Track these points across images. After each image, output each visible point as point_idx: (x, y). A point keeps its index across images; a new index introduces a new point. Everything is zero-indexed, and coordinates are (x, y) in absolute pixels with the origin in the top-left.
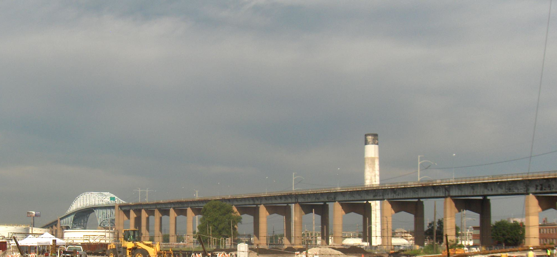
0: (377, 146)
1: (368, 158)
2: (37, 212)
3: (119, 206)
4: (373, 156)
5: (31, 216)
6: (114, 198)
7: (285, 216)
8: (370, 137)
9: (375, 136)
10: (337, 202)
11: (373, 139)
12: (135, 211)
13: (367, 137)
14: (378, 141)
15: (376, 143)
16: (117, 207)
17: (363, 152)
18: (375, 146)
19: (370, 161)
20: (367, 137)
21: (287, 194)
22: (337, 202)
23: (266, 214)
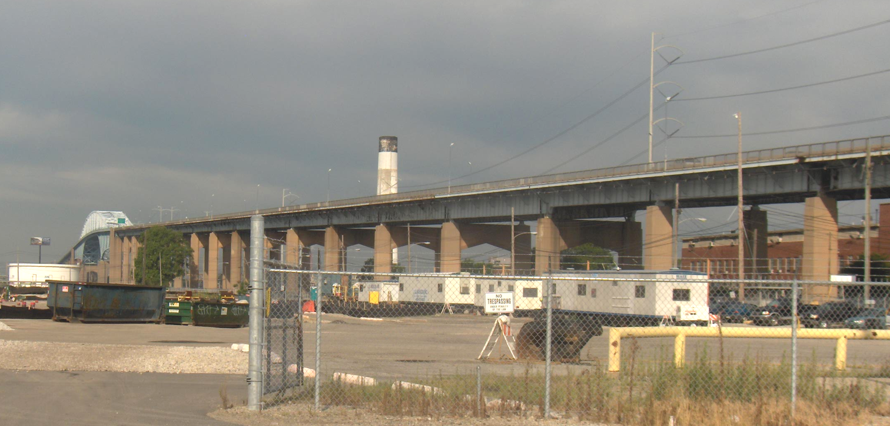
0: (394, 154)
1: (381, 170)
2: (46, 239)
3: (115, 231)
4: (388, 168)
5: (36, 244)
6: (124, 219)
7: (11, 265)
8: (385, 141)
9: (393, 140)
10: (382, 225)
11: (389, 144)
12: (219, 234)
13: (381, 141)
14: (396, 146)
15: (393, 149)
16: (112, 233)
17: (375, 162)
18: (391, 154)
19: (383, 175)
20: (381, 141)
21: (227, 218)
22: (382, 225)
23: (218, 245)
